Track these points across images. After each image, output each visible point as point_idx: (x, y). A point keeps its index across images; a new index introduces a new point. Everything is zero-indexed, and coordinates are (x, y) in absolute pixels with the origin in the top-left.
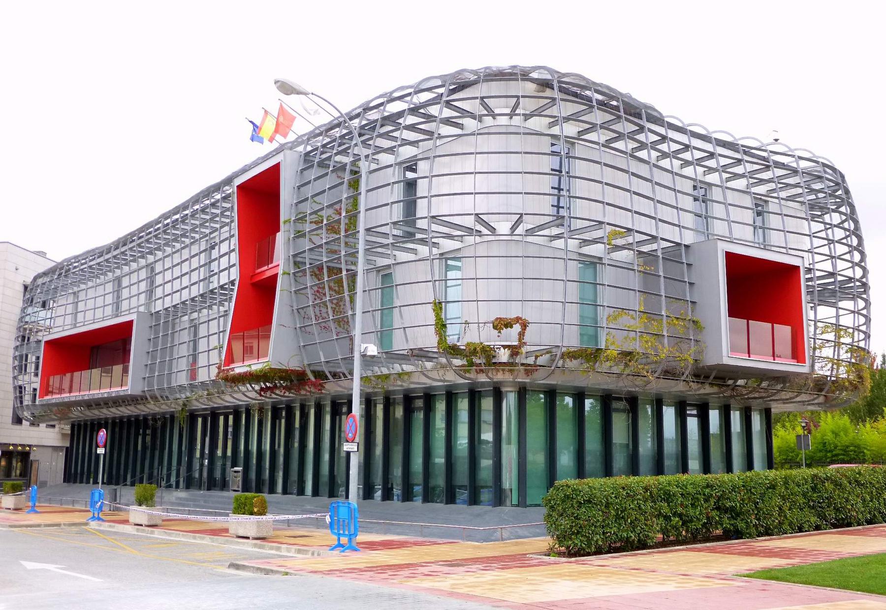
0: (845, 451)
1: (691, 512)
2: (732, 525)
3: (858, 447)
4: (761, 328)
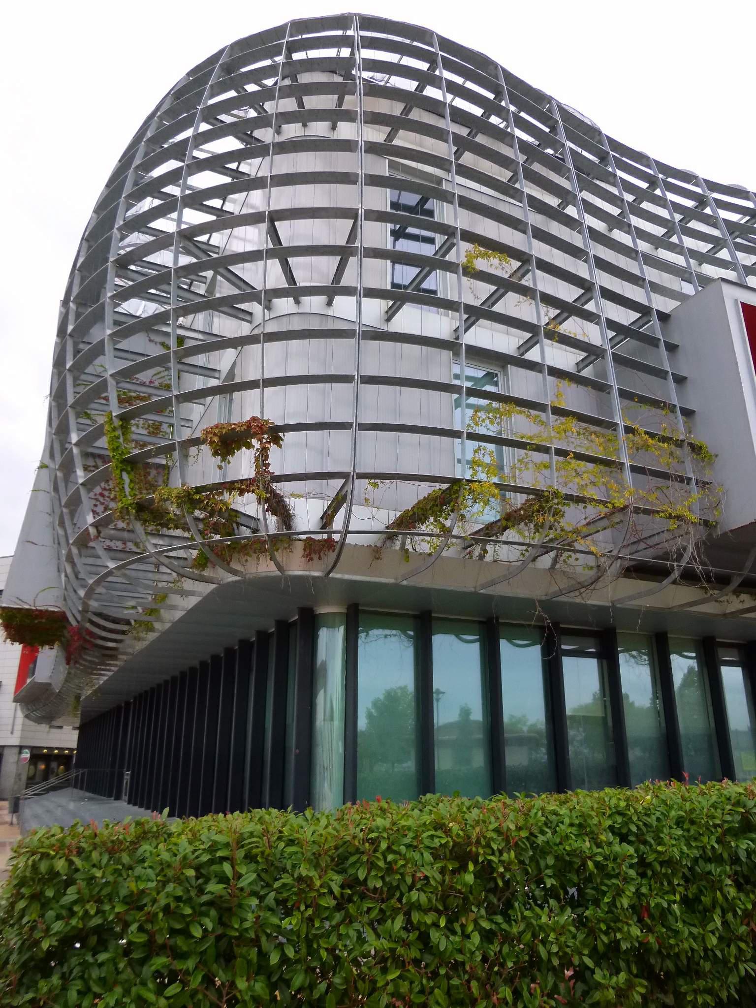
1: (686, 937)
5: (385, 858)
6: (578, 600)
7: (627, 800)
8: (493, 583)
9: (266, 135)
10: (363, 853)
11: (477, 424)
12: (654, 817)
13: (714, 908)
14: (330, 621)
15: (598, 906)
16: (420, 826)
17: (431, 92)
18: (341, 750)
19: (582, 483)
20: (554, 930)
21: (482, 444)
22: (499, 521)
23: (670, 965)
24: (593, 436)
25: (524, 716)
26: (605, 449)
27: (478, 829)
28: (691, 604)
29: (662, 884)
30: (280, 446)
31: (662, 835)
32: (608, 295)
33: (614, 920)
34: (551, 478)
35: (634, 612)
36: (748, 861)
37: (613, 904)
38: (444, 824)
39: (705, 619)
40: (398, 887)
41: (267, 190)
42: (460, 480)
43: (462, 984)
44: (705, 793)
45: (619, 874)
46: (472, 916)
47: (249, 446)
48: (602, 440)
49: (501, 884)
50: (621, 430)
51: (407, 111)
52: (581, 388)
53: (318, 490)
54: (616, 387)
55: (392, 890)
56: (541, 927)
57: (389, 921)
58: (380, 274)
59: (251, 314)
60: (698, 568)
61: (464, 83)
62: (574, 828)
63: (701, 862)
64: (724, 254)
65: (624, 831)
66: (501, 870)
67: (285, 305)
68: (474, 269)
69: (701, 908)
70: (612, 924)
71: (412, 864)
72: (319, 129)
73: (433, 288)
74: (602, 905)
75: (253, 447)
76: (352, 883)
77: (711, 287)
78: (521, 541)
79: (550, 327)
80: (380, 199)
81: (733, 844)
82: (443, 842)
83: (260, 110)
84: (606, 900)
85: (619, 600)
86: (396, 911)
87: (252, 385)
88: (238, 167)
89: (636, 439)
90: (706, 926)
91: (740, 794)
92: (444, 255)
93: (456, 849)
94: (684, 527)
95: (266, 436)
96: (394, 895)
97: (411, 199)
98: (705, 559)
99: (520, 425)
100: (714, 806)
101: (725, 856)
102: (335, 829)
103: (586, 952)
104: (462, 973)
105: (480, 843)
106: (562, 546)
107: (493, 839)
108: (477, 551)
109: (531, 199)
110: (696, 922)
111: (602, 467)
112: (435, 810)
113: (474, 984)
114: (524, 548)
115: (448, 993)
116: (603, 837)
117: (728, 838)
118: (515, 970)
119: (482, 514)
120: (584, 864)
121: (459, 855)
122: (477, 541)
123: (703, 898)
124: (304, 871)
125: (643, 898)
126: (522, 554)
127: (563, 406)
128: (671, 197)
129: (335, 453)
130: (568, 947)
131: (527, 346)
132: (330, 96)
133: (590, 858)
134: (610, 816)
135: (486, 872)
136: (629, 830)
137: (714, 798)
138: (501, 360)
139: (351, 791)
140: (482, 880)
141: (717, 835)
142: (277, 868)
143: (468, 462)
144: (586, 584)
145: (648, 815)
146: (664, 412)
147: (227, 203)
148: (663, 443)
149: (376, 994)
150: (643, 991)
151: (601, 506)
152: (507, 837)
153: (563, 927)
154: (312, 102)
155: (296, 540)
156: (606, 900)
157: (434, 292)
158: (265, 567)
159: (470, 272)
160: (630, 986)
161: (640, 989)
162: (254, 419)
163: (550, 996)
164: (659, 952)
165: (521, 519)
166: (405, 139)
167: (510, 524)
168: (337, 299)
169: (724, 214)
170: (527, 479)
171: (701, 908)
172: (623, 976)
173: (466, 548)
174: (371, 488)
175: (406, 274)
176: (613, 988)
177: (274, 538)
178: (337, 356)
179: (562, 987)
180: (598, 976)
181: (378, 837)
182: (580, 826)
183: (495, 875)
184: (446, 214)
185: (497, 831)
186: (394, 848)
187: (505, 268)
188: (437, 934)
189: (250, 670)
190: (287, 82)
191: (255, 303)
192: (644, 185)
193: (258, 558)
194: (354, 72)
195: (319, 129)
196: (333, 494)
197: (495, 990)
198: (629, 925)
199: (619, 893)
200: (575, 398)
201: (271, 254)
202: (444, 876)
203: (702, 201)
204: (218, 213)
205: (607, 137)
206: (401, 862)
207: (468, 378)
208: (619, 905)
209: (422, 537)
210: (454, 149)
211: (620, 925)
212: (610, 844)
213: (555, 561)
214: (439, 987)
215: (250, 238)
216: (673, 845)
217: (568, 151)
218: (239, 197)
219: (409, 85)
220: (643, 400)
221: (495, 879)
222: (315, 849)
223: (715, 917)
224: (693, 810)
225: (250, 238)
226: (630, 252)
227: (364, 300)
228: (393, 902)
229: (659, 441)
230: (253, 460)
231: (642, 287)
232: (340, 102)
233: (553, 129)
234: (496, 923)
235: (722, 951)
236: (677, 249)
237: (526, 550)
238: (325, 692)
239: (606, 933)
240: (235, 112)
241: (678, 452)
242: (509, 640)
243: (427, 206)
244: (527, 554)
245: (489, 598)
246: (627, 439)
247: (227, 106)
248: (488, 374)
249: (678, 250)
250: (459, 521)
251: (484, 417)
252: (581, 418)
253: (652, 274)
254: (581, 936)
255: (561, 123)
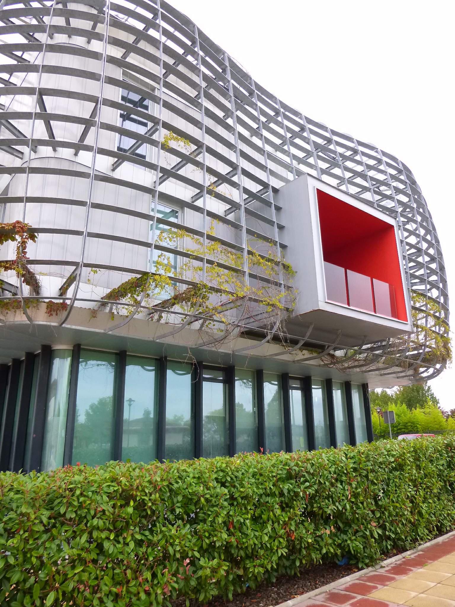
0: (405, 426)
1: (252, 537)
2: (339, 546)
3: (413, 423)
4: (359, 280)
5: (78, 499)
6: (214, 349)
7: (227, 463)
8: (164, 336)
9: (42, 37)
10: (64, 497)
11: (161, 240)
12: (241, 473)
13: (268, 521)
14: (62, 355)
15: (205, 523)
16: (102, 480)
17: (152, 32)
18: (63, 434)
19: (220, 281)
20: (178, 538)
21: (163, 252)
22: (170, 299)
23: (242, 553)
24: (229, 254)
25: (176, 416)
26: (235, 262)
27: (138, 481)
28: (276, 355)
29: (241, 509)
30: (35, 241)
31: (243, 482)
32: (246, 173)
33: (214, 530)
34: (203, 277)
35: (245, 357)
36: (289, 495)
37: (213, 521)
38: (117, 479)
39: (285, 363)
40: (85, 517)
41: (39, 74)
42: (148, 273)
43: (121, 572)
44: (270, 459)
45: (218, 504)
46: (131, 532)
47: (14, 239)
48: (234, 257)
49: (149, 513)
50: (245, 253)
51: (137, 41)
52: (225, 225)
53: (59, 272)
54: (245, 228)
55: (81, 519)
56: (171, 536)
57: (78, 538)
58: (111, 141)
59: (22, 153)
60: (281, 334)
61: (174, 32)
62: (195, 479)
63: (264, 496)
64: (311, 160)
65: (223, 480)
66: (150, 504)
67: (45, 151)
68: (168, 146)
69: (261, 521)
70: (212, 533)
71: (95, 502)
72: (79, 41)
73: (144, 154)
74: (207, 522)
75: (17, 240)
76: (56, 516)
77: (302, 177)
78: (183, 312)
79: (211, 188)
80: (115, 94)
81: (281, 486)
82: (115, 489)
83: (40, 20)
84: (210, 519)
85: (236, 350)
86: (83, 531)
87: (19, 200)
88: (22, 55)
89: (254, 259)
90: (263, 531)
91: (287, 459)
92: (151, 135)
93: (124, 494)
94: (276, 311)
95: (25, 234)
96: (83, 521)
97: (136, 97)
98: (285, 329)
99: (188, 243)
100: (273, 466)
101: (277, 493)
102: (47, 483)
103: (196, 549)
104: (122, 566)
105: (138, 489)
106: (206, 317)
107: (147, 487)
108: (156, 317)
109: (207, 110)
110: (258, 529)
111: (232, 272)
112: (113, 470)
113: (129, 572)
114: (184, 316)
115: (113, 578)
116: (211, 484)
117: (279, 483)
118: (154, 562)
119: (163, 294)
120: (199, 500)
121: (126, 497)
122: (156, 311)
123: (263, 516)
124: (24, 509)
125: (231, 517)
126: (182, 320)
127: (214, 235)
128: (286, 123)
129: (71, 248)
130: (186, 546)
131: (197, 197)
132: (88, 22)
133: (203, 496)
134: (216, 472)
135: (141, 506)
136: (227, 480)
137: (274, 461)
138: (181, 204)
139: (68, 459)
140: (137, 510)
141: (273, 481)
142: (7, 508)
143: (154, 262)
144: (219, 340)
145: (238, 472)
146: (271, 245)
147: (12, 77)
148: (268, 262)
149: (67, 582)
150: (226, 568)
151: (230, 295)
152: (155, 486)
153: (184, 536)
154: (75, 23)
155: (41, 302)
156: (210, 519)
157: (144, 157)
158: (19, 318)
159: (165, 147)
160: (219, 566)
161: (225, 566)
162: (18, 222)
163: (173, 575)
164: (237, 546)
165: (184, 299)
166: (133, 59)
167: (176, 302)
168: (81, 152)
169: (314, 138)
170: (188, 276)
171: (261, 521)
172: (216, 561)
173: (150, 314)
174: (92, 273)
175: (128, 143)
176: (210, 568)
177: (27, 300)
178: (78, 189)
179: (181, 570)
180: (202, 562)
181: (75, 487)
182: (199, 478)
183: (146, 507)
184: (155, 110)
185: (150, 482)
186: (85, 493)
187: (187, 149)
188: (108, 544)
189: (7, 384)
190: (60, 6)
191: (26, 147)
192: (272, 113)
193: (15, 312)
194: (104, 9)
195: (79, 41)
196: (68, 275)
197: (141, 575)
198: (221, 532)
199: (217, 515)
200: (222, 231)
201: (38, 116)
202: (115, 509)
203: (303, 129)
204: (5, 83)
205: (255, 82)
206: (88, 502)
207: (159, 212)
208: (217, 522)
209: (123, 306)
210: (164, 71)
211: (216, 533)
212: (215, 488)
213: (202, 325)
214: (107, 575)
215: (26, 103)
216: (249, 488)
217: (231, 86)
218: (22, 75)
219: (140, 26)
220: (259, 236)
221: (145, 510)
222: (33, 495)
223: (268, 525)
224: (262, 468)
225: (26, 103)
226: (260, 150)
227: (97, 155)
228: (82, 526)
229: (266, 261)
230: (16, 249)
231: (265, 171)
232: (94, 27)
233: (224, 70)
234: (146, 536)
235: (270, 544)
236: (286, 153)
237: (185, 318)
238: (55, 399)
239: (208, 538)
240: (23, 18)
241: (276, 268)
242: (173, 371)
243: (145, 103)
244: (185, 320)
245: (162, 345)
246: (249, 257)
247: (17, 13)
248: (173, 211)
249: (287, 153)
250: (146, 298)
251: (166, 236)
252: (223, 243)
253: (271, 165)
254: (194, 541)
255: (229, 68)
